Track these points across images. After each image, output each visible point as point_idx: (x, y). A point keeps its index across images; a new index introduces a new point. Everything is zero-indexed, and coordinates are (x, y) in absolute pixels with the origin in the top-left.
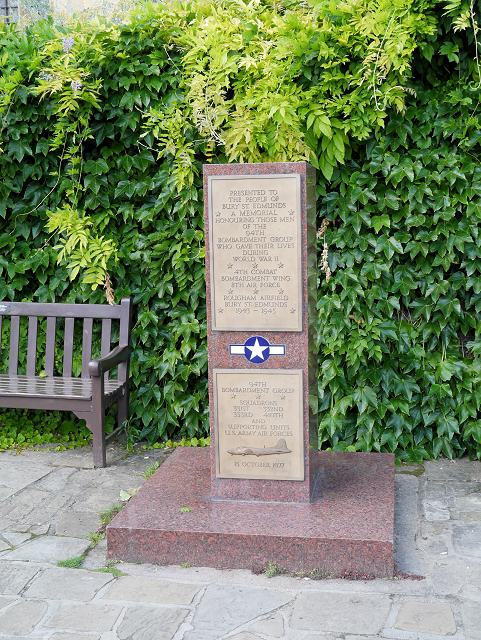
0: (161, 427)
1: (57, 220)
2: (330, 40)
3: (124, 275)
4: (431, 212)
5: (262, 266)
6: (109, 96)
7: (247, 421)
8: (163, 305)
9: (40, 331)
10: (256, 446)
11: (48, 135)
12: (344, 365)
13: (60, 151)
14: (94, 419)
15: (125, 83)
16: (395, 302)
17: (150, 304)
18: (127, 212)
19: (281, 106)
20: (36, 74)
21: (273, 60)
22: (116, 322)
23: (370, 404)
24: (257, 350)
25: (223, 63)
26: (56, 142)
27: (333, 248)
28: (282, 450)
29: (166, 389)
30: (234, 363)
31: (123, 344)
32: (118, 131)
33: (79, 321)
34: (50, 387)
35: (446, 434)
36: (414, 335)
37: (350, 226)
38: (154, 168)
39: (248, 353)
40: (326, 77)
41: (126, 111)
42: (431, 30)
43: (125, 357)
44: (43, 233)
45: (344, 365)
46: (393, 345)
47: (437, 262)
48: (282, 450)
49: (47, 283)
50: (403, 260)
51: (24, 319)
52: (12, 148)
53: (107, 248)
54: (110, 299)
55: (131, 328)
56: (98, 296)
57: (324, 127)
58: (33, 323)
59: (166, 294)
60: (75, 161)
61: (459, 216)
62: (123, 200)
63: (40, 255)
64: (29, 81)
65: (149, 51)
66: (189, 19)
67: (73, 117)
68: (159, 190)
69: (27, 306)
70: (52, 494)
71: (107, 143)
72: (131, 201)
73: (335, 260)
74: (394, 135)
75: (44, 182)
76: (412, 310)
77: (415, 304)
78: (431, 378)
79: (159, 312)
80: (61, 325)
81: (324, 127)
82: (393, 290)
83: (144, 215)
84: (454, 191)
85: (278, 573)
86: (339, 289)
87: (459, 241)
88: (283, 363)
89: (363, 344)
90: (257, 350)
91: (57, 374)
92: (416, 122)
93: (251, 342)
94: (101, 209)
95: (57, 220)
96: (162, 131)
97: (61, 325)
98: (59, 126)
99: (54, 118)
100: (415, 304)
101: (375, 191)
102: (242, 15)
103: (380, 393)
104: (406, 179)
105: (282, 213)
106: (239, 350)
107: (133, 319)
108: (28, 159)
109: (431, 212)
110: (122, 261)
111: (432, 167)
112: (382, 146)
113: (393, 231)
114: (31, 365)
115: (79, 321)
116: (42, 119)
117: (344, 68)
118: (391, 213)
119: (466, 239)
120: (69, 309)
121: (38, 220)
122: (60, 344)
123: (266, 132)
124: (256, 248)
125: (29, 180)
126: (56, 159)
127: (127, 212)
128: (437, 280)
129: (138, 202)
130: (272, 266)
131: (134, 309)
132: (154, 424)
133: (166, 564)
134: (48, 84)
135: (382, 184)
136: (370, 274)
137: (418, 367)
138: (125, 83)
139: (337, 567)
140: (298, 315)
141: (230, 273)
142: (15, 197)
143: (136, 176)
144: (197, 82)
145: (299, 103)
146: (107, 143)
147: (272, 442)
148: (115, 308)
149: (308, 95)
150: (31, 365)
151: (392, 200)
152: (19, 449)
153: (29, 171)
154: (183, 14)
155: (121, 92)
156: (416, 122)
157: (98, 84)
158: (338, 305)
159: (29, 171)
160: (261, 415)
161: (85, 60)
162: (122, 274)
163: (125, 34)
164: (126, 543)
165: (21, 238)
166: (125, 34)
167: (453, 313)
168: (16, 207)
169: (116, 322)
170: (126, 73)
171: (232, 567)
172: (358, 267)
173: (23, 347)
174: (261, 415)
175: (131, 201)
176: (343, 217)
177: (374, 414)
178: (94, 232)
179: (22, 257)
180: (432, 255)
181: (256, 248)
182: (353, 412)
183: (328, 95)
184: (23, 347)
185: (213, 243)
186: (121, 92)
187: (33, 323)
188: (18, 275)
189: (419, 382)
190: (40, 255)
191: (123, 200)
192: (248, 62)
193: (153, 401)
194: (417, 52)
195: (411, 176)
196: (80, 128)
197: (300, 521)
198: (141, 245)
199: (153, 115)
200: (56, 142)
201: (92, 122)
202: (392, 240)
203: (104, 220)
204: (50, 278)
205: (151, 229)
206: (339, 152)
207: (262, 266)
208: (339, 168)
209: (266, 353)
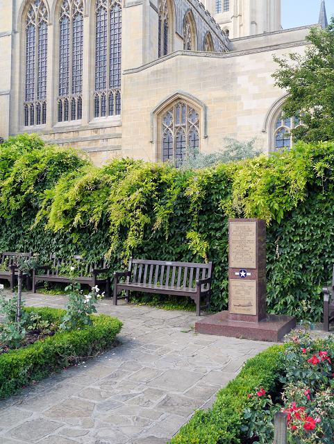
0: (221, 306)
1: (190, 235)
2: (278, 179)
3: (211, 254)
4: (313, 235)
5: (245, 248)
6: (209, 195)
7: (239, 295)
8: (223, 265)
9: (183, 272)
10: (242, 304)
11: (188, 207)
12: (283, 287)
13: (191, 213)
14: (197, 301)
15: (213, 191)
16: (301, 266)
17: (219, 264)
18: (213, 233)
19: (260, 201)
20: (185, 188)
21: (260, 184)
22: (207, 270)
23: (291, 301)
24: (243, 274)
25: (245, 186)
26: (191, 210)
27: (280, 247)
28: (250, 305)
29: (223, 293)
30: (236, 278)
31: (209, 277)
32: (211, 207)
33: (195, 269)
34: (184, 289)
35: (318, 313)
36: (309, 278)
37: (285, 239)
38: (223, 219)
39: (240, 275)
40: (277, 191)
41: (213, 200)
42: (311, 176)
43: (209, 281)
44: (185, 239)
45: (283, 287)
46: (300, 280)
47: (315, 252)
48: (250, 305)
49: (186, 256)
50: (303, 252)
51: (177, 267)
52: (177, 211)
53: (205, 244)
54: (206, 262)
55: (212, 272)
56: (202, 260)
57: (276, 206)
58: (180, 269)
59: (224, 261)
60: (196, 216)
61: (323, 237)
62: (211, 229)
63: (183, 246)
64: (183, 190)
65: (221, 181)
66: (236, 170)
67: (196, 202)
68: (224, 226)
69: (179, 263)
70: (182, 320)
71: (207, 210)
72: (214, 229)
73: (281, 251)
74: (301, 209)
75: (186, 222)
76: (307, 269)
77: (308, 267)
78: (314, 293)
79: (222, 267)
80: (189, 270)
81: (276, 206)
82: (301, 261)
83: (218, 234)
84: (321, 228)
85: (243, 338)
86: (282, 260)
87: (322, 245)
88: (250, 278)
89: (289, 279)
90: (243, 274)
91: (187, 286)
92: (310, 205)
93: (241, 271)
94: (205, 232)
95: (190, 235)
96: (225, 207)
97: (189, 270)
98: (191, 205)
99: (190, 203)
100: (308, 267)
101: (294, 228)
102: (252, 170)
103: (295, 298)
104: (304, 224)
105: (250, 233)
106: (238, 274)
107: (213, 270)
108: (182, 215)
109: (313, 235)
110: (210, 249)
111: (314, 219)
112: (297, 212)
113: (300, 241)
114: (179, 283)
115: (195, 269)
116: (187, 202)
117: (283, 188)
118: (300, 235)
119: (329, 243)
120: (192, 265)
121: (184, 235)
122: (188, 277)
123: (256, 208)
124: (243, 243)
125: (182, 222)
126: (189, 216)
127: (213, 233)
128: (316, 259)
129: (217, 230)
130: (247, 249)
131: (214, 266)
132: (218, 305)
133: (212, 334)
134: (189, 192)
135: (297, 227)
136: (292, 255)
137: (309, 289)
138: (213, 191)
139: (261, 338)
140: (255, 264)
141: (235, 250)
142: (177, 227)
143: (216, 221)
144: (235, 192)
145: (268, 199)
146: (207, 210)
147: (246, 303)
148: (207, 265)
149: (271, 196)
150: (179, 283)
151: (300, 231)
152: (173, 310)
153: (181, 219)
154: (234, 168)
155: (212, 194)
156: (310, 205)
157: (204, 192)
158: (281, 266)
159: (181, 219)
160: (243, 294)
161: (201, 184)
162: (210, 254)
163: (214, 175)
164: (199, 328)
165: (178, 241)
166: (214, 175)
167: (321, 270)
168: (177, 231)
169: (207, 270)
170: (213, 188)
171: (230, 336)
172: (288, 253)
173: (176, 277)
174: (243, 294)
175: (214, 229)
176: (283, 236)
177: (293, 305)
178: (201, 239)
179: (178, 247)
180: (313, 250)
181: (243, 243)
182: (285, 303)
183: (278, 196)
184: (176, 277)
185: (230, 242)
186: (212, 194)
187: (180, 269)
188: (176, 253)
189: (309, 294)
190: (183, 246)
191: (211, 229)
192: (252, 185)
193: (218, 297)
194: (307, 183)
195: (306, 223)
196: (198, 206)
197: (255, 325)
198: (217, 244)
199: (222, 201)
200: (191, 210)
201: (202, 204)
202: (300, 244)
203: (205, 235)
204: (187, 254)
205: (221, 239)
206: (281, 215)
207: (245, 248)
208: (282, 220)
209: (245, 275)
